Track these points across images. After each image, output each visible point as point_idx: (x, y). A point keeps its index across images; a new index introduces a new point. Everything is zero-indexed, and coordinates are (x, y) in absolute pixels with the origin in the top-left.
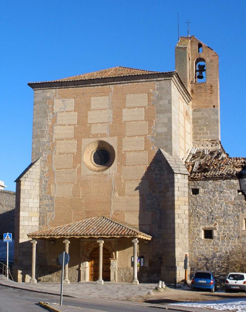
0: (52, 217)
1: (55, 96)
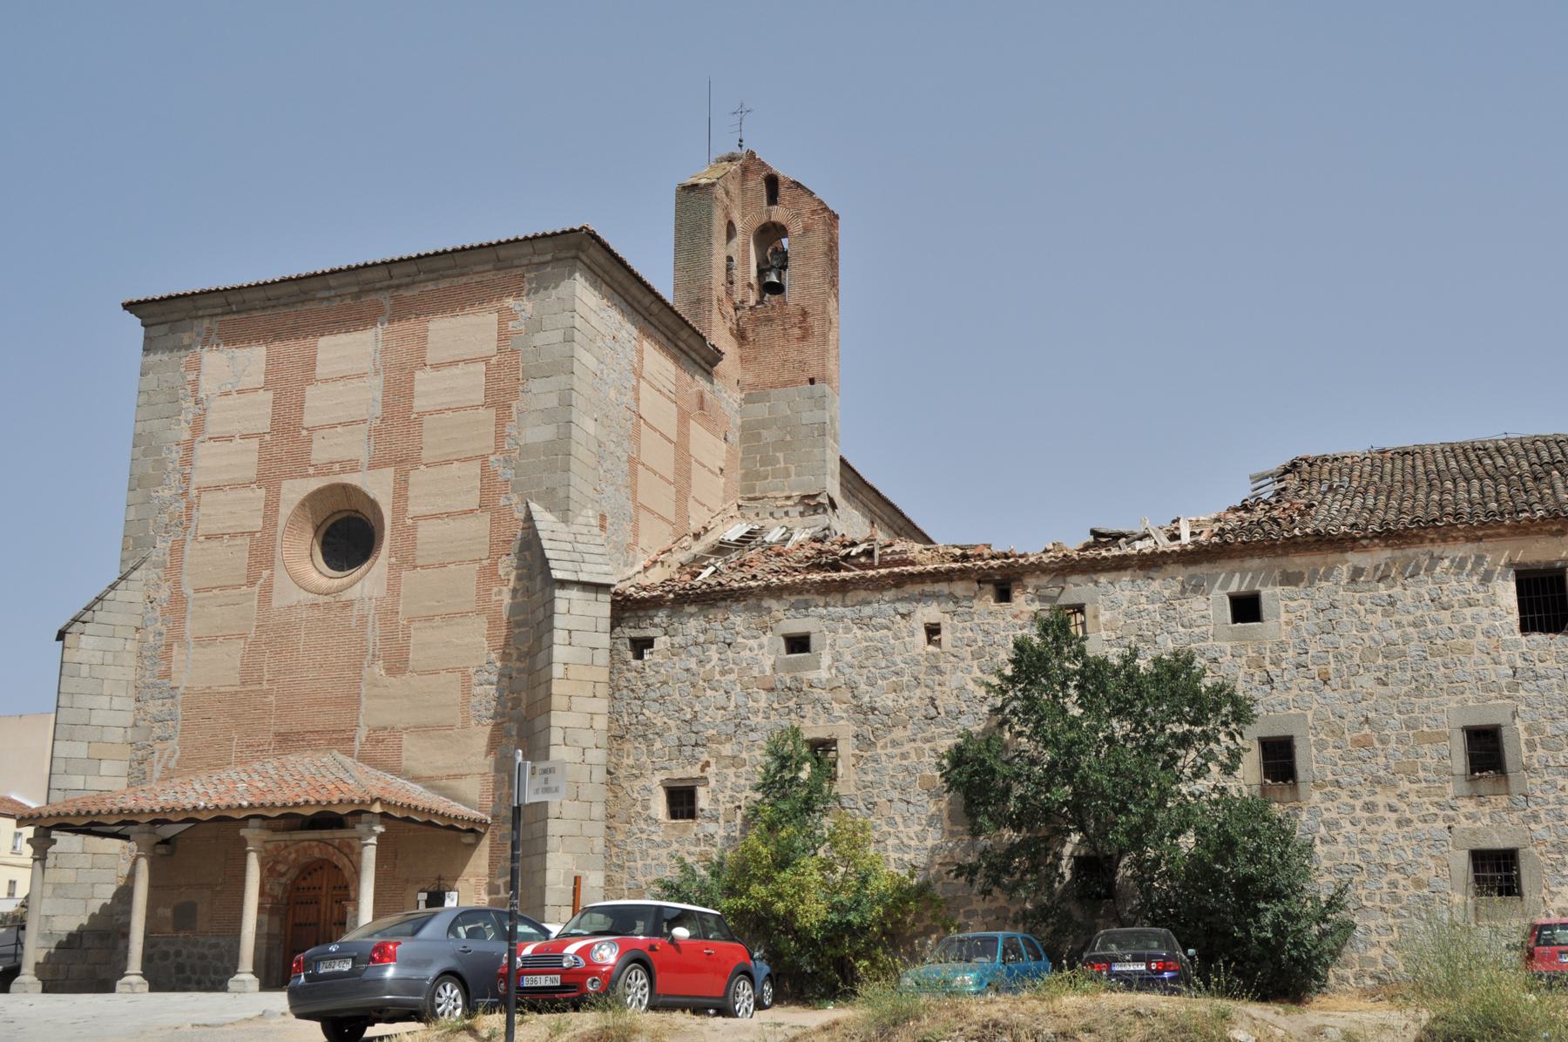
0: (170, 757)
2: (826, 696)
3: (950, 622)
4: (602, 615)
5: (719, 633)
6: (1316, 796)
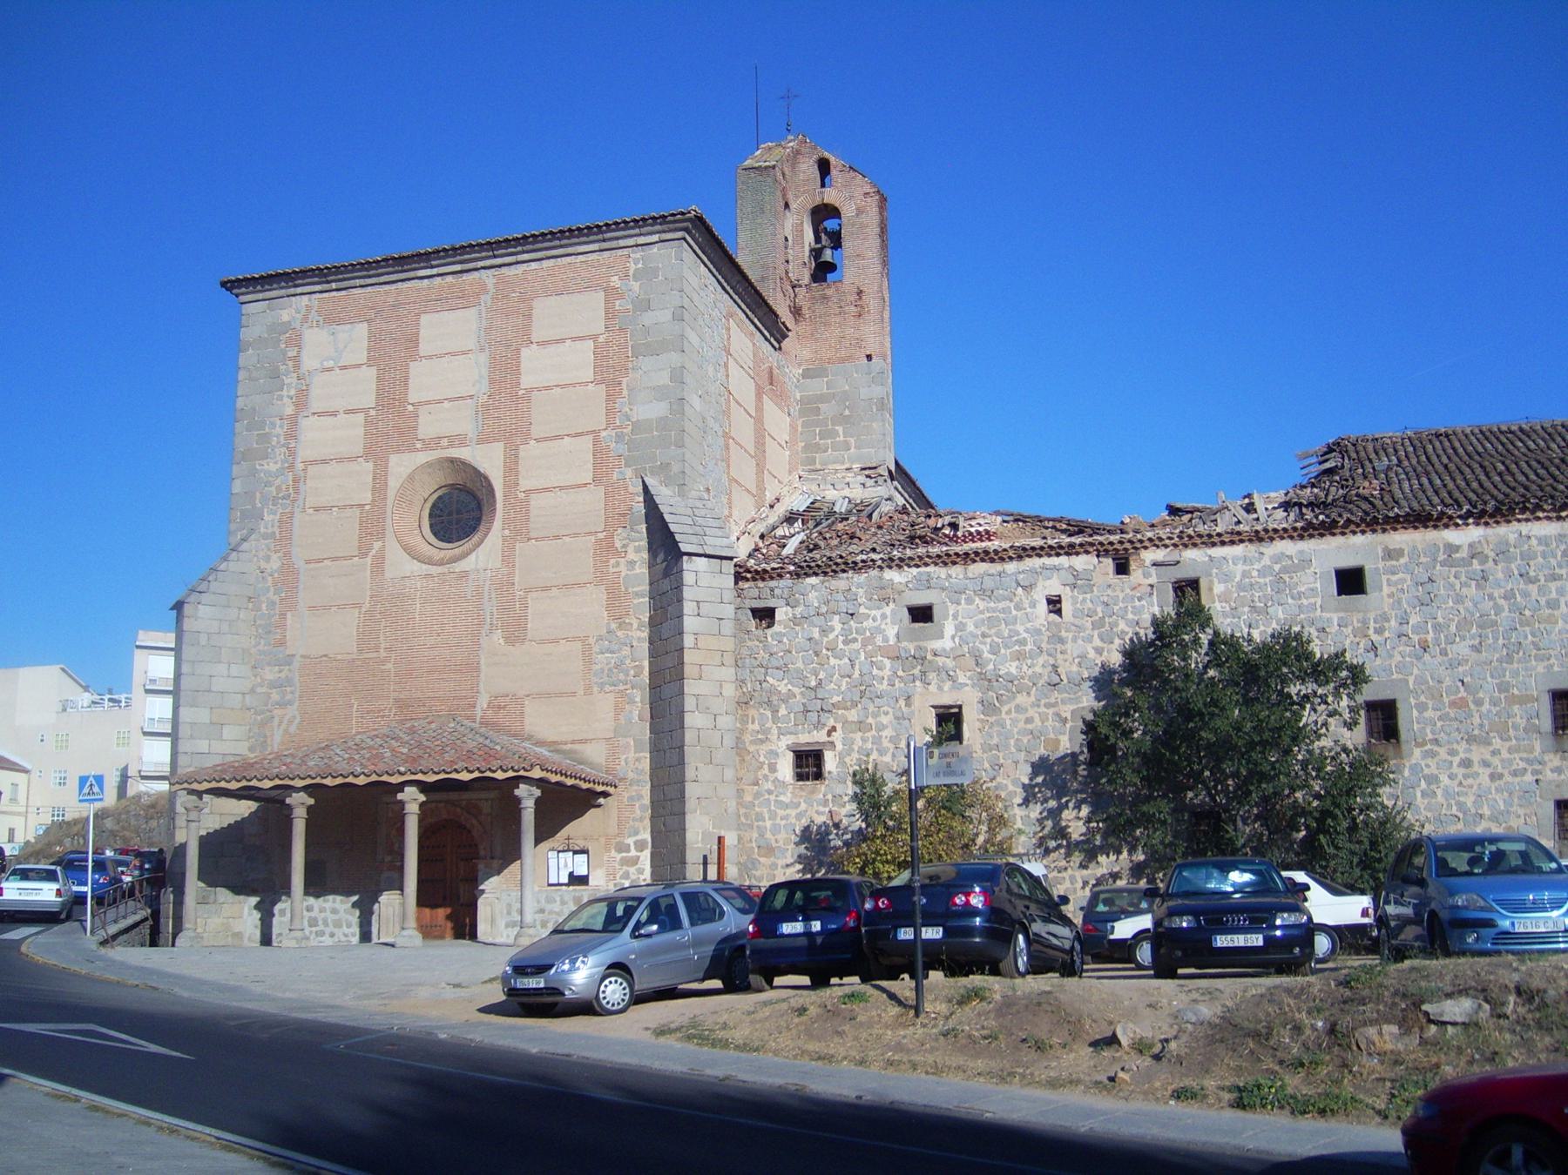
0: (290, 722)
1: (305, 319)
2: (950, 663)
3: (1070, 594)
4: (727, 586)
5: (841, 604)
6: (1417, 752)
